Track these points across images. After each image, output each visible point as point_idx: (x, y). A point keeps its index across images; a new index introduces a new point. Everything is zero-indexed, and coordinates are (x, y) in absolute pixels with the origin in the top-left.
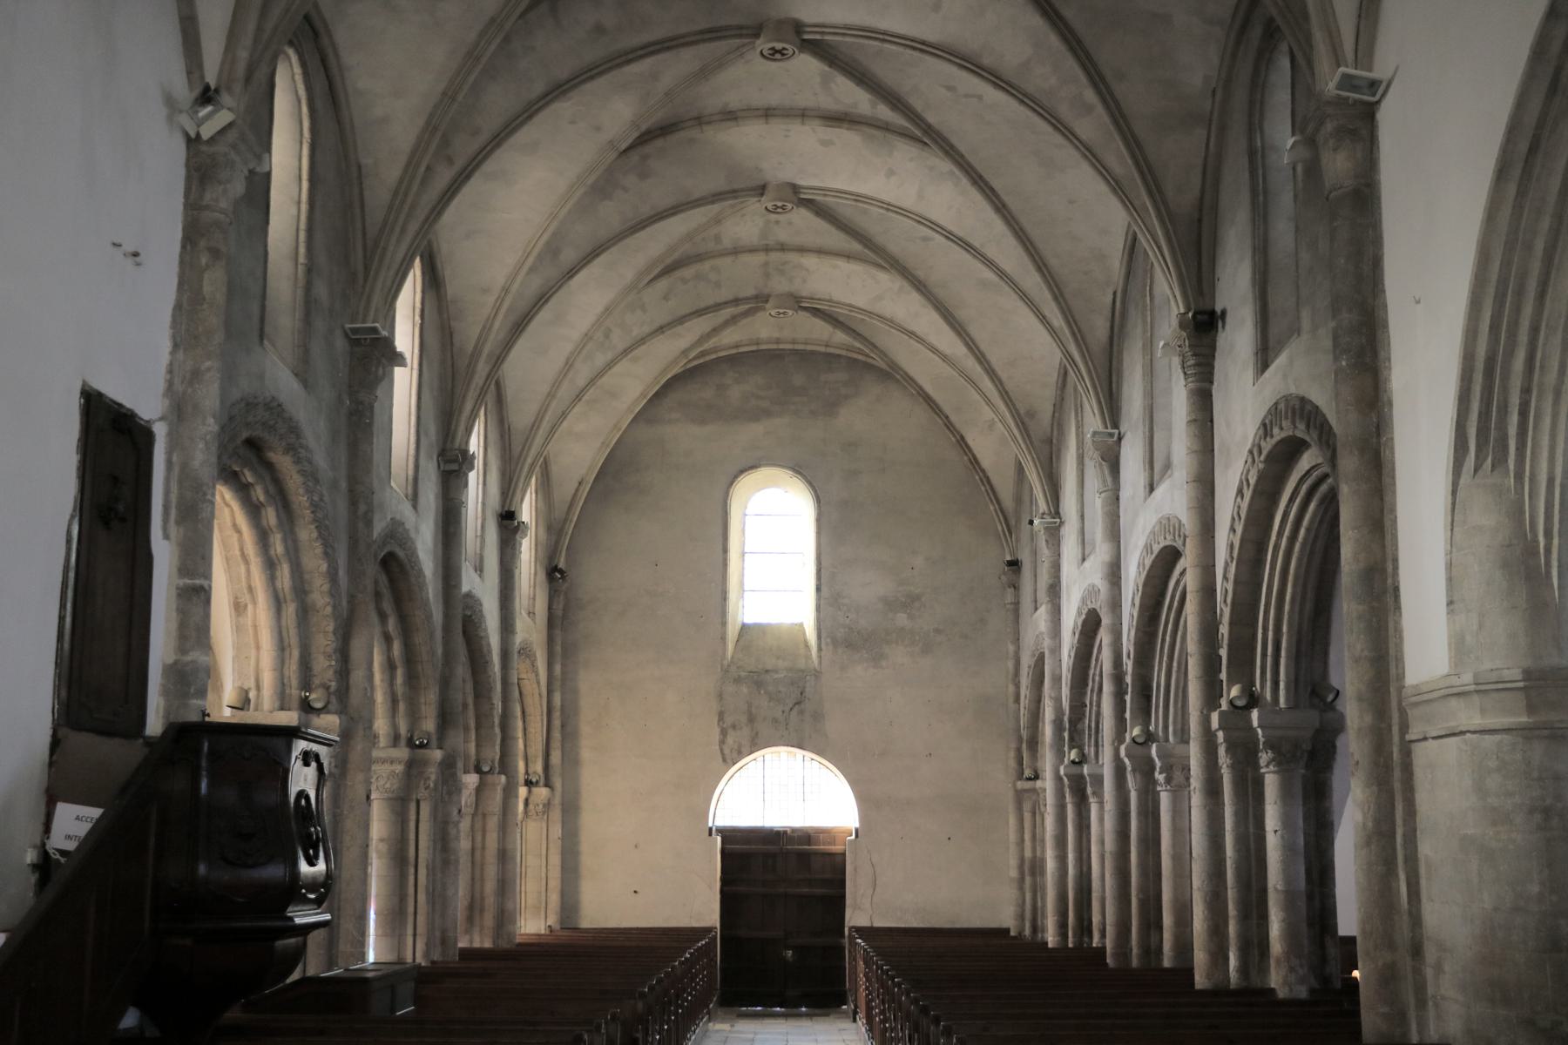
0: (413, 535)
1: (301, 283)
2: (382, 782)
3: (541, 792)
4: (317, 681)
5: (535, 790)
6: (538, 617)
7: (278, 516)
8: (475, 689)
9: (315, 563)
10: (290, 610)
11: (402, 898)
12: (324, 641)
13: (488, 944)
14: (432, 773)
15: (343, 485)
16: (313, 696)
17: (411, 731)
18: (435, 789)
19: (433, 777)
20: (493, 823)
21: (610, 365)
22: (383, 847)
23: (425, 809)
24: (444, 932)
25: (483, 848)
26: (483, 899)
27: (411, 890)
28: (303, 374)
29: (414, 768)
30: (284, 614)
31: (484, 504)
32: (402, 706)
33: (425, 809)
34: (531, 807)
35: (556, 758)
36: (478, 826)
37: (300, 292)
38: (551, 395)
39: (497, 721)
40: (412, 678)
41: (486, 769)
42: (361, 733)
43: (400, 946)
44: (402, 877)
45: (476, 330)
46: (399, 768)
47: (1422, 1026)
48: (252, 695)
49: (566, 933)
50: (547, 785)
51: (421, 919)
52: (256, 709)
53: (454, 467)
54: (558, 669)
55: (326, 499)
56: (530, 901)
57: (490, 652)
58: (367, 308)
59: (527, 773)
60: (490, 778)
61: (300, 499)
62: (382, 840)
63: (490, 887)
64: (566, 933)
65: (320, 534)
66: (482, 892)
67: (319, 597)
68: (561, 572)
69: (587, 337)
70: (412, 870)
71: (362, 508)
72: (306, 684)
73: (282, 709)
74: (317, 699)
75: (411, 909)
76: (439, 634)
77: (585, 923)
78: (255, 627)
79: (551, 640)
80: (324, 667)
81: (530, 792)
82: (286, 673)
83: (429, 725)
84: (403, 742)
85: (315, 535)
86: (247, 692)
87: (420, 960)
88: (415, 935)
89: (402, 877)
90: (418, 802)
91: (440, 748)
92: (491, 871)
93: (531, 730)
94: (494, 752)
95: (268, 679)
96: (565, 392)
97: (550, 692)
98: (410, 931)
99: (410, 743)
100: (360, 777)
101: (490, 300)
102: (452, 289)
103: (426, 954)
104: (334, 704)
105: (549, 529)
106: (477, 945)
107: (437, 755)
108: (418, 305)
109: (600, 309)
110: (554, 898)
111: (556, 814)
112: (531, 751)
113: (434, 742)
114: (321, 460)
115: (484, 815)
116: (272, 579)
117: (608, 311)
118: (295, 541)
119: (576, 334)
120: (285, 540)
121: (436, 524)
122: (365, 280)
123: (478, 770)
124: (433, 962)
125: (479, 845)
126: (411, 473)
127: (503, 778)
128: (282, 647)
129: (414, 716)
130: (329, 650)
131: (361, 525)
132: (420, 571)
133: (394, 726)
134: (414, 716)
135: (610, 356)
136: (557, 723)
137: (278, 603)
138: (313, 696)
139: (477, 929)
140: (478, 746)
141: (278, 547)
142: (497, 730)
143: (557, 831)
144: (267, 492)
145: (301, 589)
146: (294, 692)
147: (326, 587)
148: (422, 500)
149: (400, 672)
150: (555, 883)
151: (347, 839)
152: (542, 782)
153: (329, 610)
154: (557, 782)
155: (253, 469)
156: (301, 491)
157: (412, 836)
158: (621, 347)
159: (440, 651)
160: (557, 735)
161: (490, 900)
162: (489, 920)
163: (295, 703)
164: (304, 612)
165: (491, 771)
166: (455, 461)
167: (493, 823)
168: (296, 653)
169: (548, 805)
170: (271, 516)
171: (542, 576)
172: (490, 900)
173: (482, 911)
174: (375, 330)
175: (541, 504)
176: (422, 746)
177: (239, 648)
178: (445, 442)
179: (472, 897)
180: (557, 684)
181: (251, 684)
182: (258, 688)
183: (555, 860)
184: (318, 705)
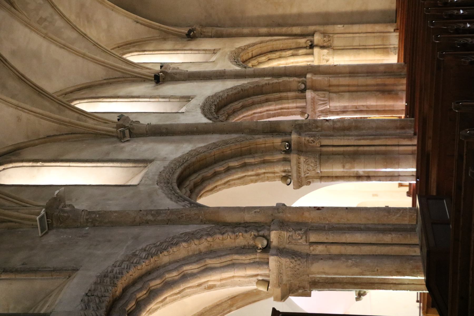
0: (166, 163)
1: (12, 276)
2: (311, 168)
3: (317, 38)
4: (251, 242)
5: (316, 42)
6: (217, 47)
7: (154, 279)
8: (257, 94)
9: (182, 250)
10: (210, 262)
11: (377, 153)
12: (228, 240)
13: (404, 81)
14: (305, 139)
15: (136, 230)
16: (260, 246)
17: (281, 151)
18: (314, 136)
19: (307, 138)
20: (334, 81)
21: (62, 16)
22: (348, 166)
23: (326, 142)
24: (397, 128)
25: (349, 86)
26: (378, 85)
27: (373, 148)
28: (70, 271)
29: (302, 150)
30: (213, 265)
31: (151, 97)
32: (267, 158)
33: (326, 142)
34: (325, 44)
35: (297, 30)
36: (335, 89)
37: (18, 276)
38: (84, 56)
39: (275, 81)
40: (250, 152)
41: (303, 86)
42: (281, 215)
43: (405, 154)
44: (365, 154)
45: (44, 122)
46: (302, 159)
47: (398, 112)
48: (260, 278)
49: (398, 21)
50: (312, 35)
51: (389, 142)
52: (269, 276)
53: (127, 132)
54: (246, 31)
55: (144, 246)
56: (380, 43)
57: (235, 88)
58: (29, 220)
59: (305, 48)
60: (308, 84)
61: (144, 266)
62: (344, 167)
63: (370, 81)
64: (398, 21)
65: (165, 249)
66: (374, 85)
67: (203, 245)
68: (190, 31)
69: (45, 37)
70: (361, 149)
71: (150, 217)
72: (253, 249)
73: (268, 263)
74: (262, 243)
75: (383, 148)
76: (225, 137)
77: (394, 6)
78: (221, 280)
79: (229, 36)
80: (243, 239)
81: (317, 46)
82: (247, 262)
83: (277, 141)
84: (287, 156)
85: (165, 253)
86: (259, 280)
87: (415, 142)
88: (399, 145)
89: (365, 154)
90: (322, 146)
91: (290, 134)
92: (361, 81)
93: (281, 47)
94: (294, 80)
95: (250, 272)
96: (80, 46)
97: (259, 35)
98: (396, 148)
99: (288, 152)
100: (306, 214)
101: (24, 116)
102: (20, 139)
103: (410, 138)
104: (265, 232)
105: (165, 39)
106: (404, 87)
107: (294, 137)
108: (31, 164)
109: (27, 30)
110: (378, 28)
111: (329, 28)
112: (294, 46)
113: (287, 138)
114: (120, 253)
115: (330, 86)
116: (193, 276)
117: (27, 25)
118: (170, 263)
119: (45, 43)
120: (170, 271)
121: (162, 142)
122: (11, 221)
123: (304, 91)
124: (415, 134)
125: (347, 88)
126: (131, 165)
127: (309, 76)
128: (233, 265)
129: (273, 150)
130: (233, 236)
131: (159, 218)
132: (189, 154)
133: (279, 161)
134: (273, 150)
135: (57, 17)
136: (277, 30)
137: (207, 270)
138: (260, 246)
139: (395, 88)
140: (290, 91)
141: (174, 275)
142: (281, 80)
143: (339, 28)
144: (141, 290)
145: (199, 257)
146: (258, 256)
147: (197, 242)
148: (147, 156)
149: (247, 161)
150: (369, 28)
151: (343, 221)
152: (310, 38)
153: (209, 239)
154: (311, 28)
155: (126, 304)
156: (139, 267)
157: (342, 149)
158: (50, 10)
159: (234, 136)
160: (284, 30)
161: (379, 81)
162: (390, 81)
163: (265, 256)
164: (212, 253)
165: (304, 83)
166: (123, 132)
167: (334, 81)
168: (236, 257)
169: (324, 34)
170: (155, 283)
171: (193, 45)
172: (379, 81)
173: (385, 85)
174: (41, 219)
175: (151, 47)
176: (290, 146)
177: (234, 285)
178: (113, 136)
179: (377, 91)
180: (254, 30)
181: (255, 279)
182: (257, 275)
183: (356, 28)
184: (265, 242)
